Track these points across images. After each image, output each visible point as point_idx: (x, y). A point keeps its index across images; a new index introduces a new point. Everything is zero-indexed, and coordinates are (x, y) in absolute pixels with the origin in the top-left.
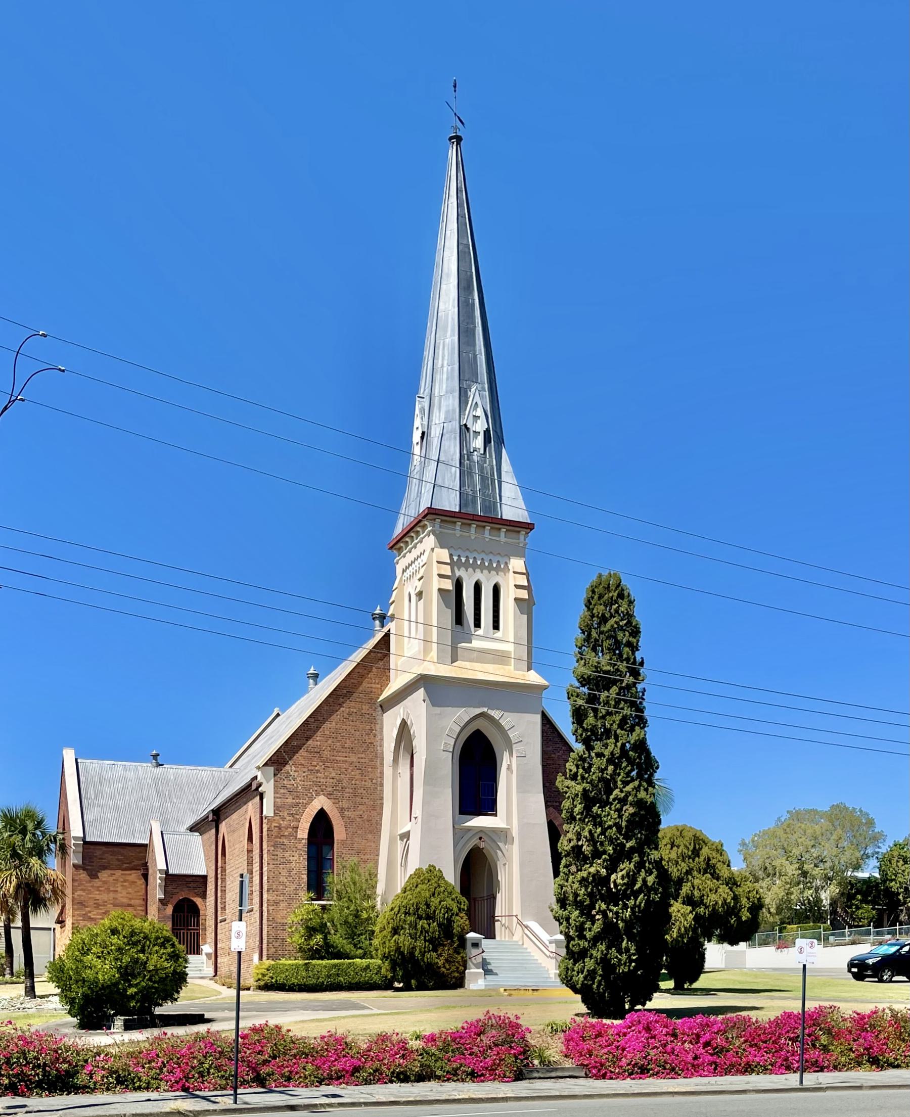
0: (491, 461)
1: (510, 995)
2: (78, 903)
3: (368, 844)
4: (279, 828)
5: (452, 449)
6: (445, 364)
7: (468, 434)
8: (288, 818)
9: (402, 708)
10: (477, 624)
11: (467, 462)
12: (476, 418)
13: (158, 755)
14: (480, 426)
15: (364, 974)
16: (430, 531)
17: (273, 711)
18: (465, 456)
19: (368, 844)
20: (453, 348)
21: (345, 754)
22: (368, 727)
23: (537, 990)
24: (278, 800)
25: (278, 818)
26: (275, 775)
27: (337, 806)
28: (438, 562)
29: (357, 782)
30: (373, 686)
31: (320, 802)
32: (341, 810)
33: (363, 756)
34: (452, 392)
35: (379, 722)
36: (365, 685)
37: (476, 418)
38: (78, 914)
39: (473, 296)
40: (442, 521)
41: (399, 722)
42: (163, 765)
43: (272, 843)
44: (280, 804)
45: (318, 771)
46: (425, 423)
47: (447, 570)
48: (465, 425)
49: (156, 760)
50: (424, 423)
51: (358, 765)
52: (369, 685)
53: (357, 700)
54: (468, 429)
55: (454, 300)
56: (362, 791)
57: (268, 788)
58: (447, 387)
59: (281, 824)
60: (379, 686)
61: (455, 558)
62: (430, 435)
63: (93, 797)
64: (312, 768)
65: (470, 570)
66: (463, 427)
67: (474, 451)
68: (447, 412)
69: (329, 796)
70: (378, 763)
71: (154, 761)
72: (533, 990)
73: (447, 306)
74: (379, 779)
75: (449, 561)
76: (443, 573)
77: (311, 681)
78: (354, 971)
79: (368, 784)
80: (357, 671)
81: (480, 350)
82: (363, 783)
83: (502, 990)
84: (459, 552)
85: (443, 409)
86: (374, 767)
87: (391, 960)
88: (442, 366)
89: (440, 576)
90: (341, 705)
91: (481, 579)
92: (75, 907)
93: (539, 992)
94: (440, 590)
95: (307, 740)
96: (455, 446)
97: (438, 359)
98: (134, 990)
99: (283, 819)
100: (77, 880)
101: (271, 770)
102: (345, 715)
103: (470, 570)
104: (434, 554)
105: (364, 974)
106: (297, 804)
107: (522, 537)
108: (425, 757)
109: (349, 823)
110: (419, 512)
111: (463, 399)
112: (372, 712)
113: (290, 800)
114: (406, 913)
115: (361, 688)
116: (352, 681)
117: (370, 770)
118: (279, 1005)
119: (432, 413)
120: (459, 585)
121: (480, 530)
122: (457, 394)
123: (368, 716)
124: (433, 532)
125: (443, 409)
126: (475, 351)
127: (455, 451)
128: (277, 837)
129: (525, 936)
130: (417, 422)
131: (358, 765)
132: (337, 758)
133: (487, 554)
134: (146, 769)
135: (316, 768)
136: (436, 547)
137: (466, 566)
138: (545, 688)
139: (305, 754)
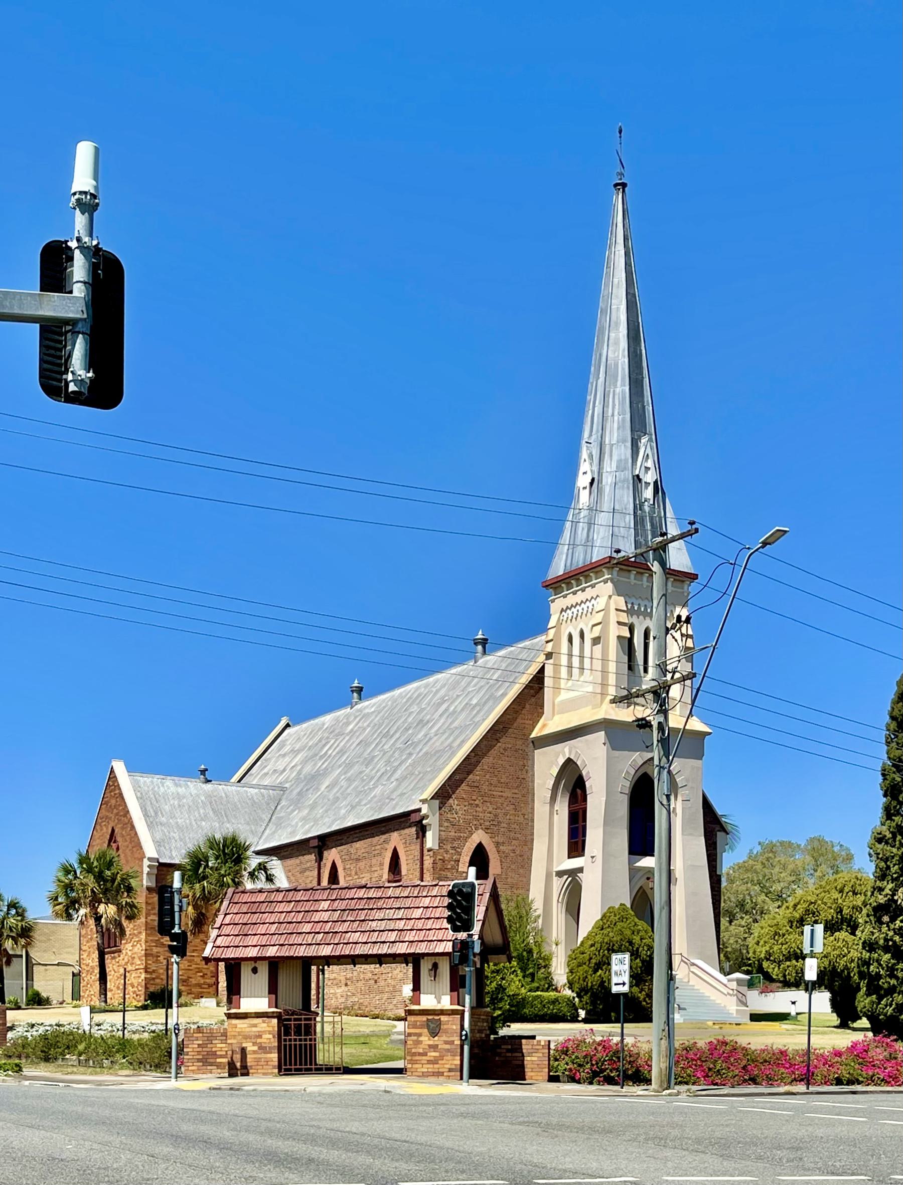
0: (659, 512)
1: (721, 1028)
2: (152, 928)
3: (520, 879)
4: (443, 861)
5: (625, 499)
6: (616, 413)
7: (639, 485)
8: (451, 851)
9: (568, 747)
10: (646, 671)
11: (639, 512)
12: (647, 469)
13: (206, 770)
14: (650, 477)
15: (551, 1007)
16: (608, 579)
17: (280, 720)
18: (638, 506)
19: (520, 879)
20: (624, 398)
21: (500, 789)
22: (521, 763)
23: (739, 1024)
24: (442, 833)
25: (442, 850)
26: (440, 808)
27: (494, 840)
28: (617, 610)
29: (511, 817)
30: (527, 722)
31: (479, 837)
32: (497, 844)
33: (516, 791)
34: (624, 441)
35: (530, 757)
36: (519, 720)
37: (647, 469)
38: (151, 940)
39: (640, 346)
40: (620, 569)
41: (561, 761)
42: (211, 781)
43: (437, 876)
44: (444, 837)
45: (477, 805)
46: (595, 469)
47: (624, 618)
48: (638, 476)
49: (205, 776)
50: (593, 469)
51: (512, 800)
52: (524, 721)
53: (512, 735)
54: (640, 480)
55: (624, 350)
56: (515, 826)
57: (433, 821)
58: (618, 435)
59: (444, 857)
60: (531, 722)
61: (629, 606)
62: (602, 483)
63: (153, 814)
64: (473, 802)
65: (641, 617)
66: (636, 478)
67: (645, 501)
68: (619, 461)
69: (486, 830)
70: (530, 799)
71: (202, 777)
72: (736, 1024)
73: (616, 354)
74: (530, 815)
75: (625, 609)
76: (621, 620)
77: (355, 695)
78: (541, 1003)
79: (521, 819)
80: (512, 706)
81: (648, 401)
82: (516, 818)
83: (710, 1023)
84: (634, 600)
85: (615, 458)
86: (526, 803)
87: (593, 993)
88: (613, 415)
89: (619, 623)
90: (498, 741)
91: (635, 623)
92: (148, 932)
93: (740, 1027)
94: (619, 637)
95: (468, 775)
96: (628, 495)
97: (608, 407)
98: (500, 1012)
99: (447, 852)
100: (150, 904)
101: (437, 802)
102: (502, 750)
103: (641, 617)
104: (612, 601)
105: (551, 1007)
106: (459, 838)
107: (686, 587)
108: (605, 799)
109: (503, 856)
110: (591, 560)
111: (634, 449)
112: (525, 748)
113: (453, 834)
114: (608, 950)
115: (515, 725)
116: (508, 716)
117: (522, 805)
118: (557, 1032)
119: (603, 461)
120: (631, 629)
121: (639, 576)
122: (629, 444)
123: (521, 752)
124: (612, 580)
125: (615, 458)
126: (643, 402)
127: (628, 501)
128: (440, 870)
129: (691, 974)
130: (584, 466)
131: (512, 800)
132: (494, 793)
133: (637, 599)
134: (194, 788)
135: (476, 802)
136: (613, 594)
137: (638, 613)
138: (710, 733)
139: (466, 788)
